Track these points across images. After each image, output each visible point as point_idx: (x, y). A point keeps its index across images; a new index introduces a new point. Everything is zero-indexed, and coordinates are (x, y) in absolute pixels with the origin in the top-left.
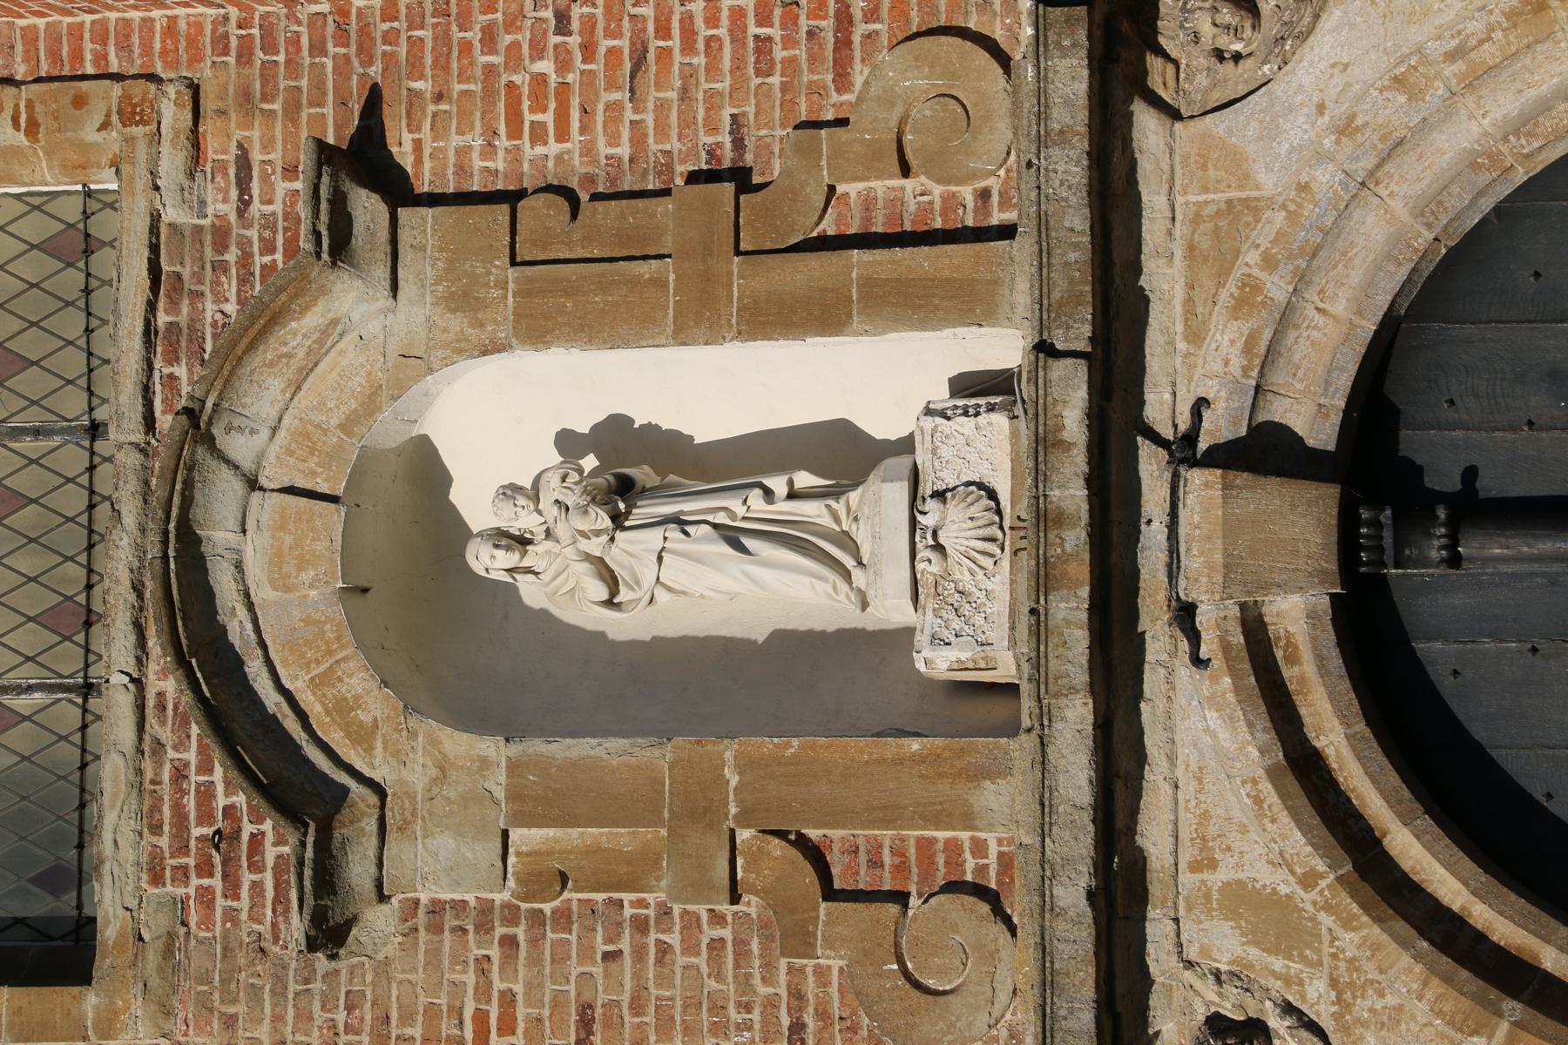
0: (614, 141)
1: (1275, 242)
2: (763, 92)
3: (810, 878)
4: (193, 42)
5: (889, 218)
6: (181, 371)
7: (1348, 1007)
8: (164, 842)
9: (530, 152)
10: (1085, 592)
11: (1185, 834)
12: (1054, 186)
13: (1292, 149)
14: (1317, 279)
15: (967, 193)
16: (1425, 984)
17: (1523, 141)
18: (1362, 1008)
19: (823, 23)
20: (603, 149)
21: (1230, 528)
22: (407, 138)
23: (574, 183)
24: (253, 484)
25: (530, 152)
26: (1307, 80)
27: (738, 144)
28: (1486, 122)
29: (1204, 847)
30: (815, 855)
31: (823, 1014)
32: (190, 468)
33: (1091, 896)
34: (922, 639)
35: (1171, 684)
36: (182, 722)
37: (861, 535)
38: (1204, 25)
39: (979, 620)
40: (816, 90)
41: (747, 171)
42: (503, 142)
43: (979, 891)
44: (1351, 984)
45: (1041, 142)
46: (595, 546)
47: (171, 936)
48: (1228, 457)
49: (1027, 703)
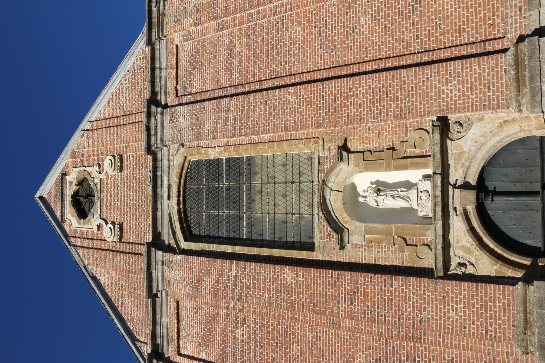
0: (376, 144)
2: (396, 137)
3: (404, 243)
4: (323, 133)
5: (413, 154)
6: (322, 175)
7: (477, 262)
8: (322, 234)
9: (366, 146)
10: (441, 206)
11: (455, 238)
15: (424, 151)
18: (479, 262)
20: (375, 145)
21: (461, 197)
22: (350, 144)
23: (371, 150)
24: (331, 190)
25: (366, 146)
26: (470, 136)
27: (393, 144)
29: (458, 240)
30: (405, 240)
31: (406, 260)
32: (323, 188)
33: (442, 247)
34: (419, 211)
35: (453, 218)
36: (323, 220)
37: (411, 197)
38: (456, 128)
39: (427, 209)
40: (403, 137)
41: (394, 148)
42: (362, 145)
43: (427, 245)
45: (433, 145)
46: (375, 198)
47: (323, 246)
48: (461, 187)
49: (433, 219)
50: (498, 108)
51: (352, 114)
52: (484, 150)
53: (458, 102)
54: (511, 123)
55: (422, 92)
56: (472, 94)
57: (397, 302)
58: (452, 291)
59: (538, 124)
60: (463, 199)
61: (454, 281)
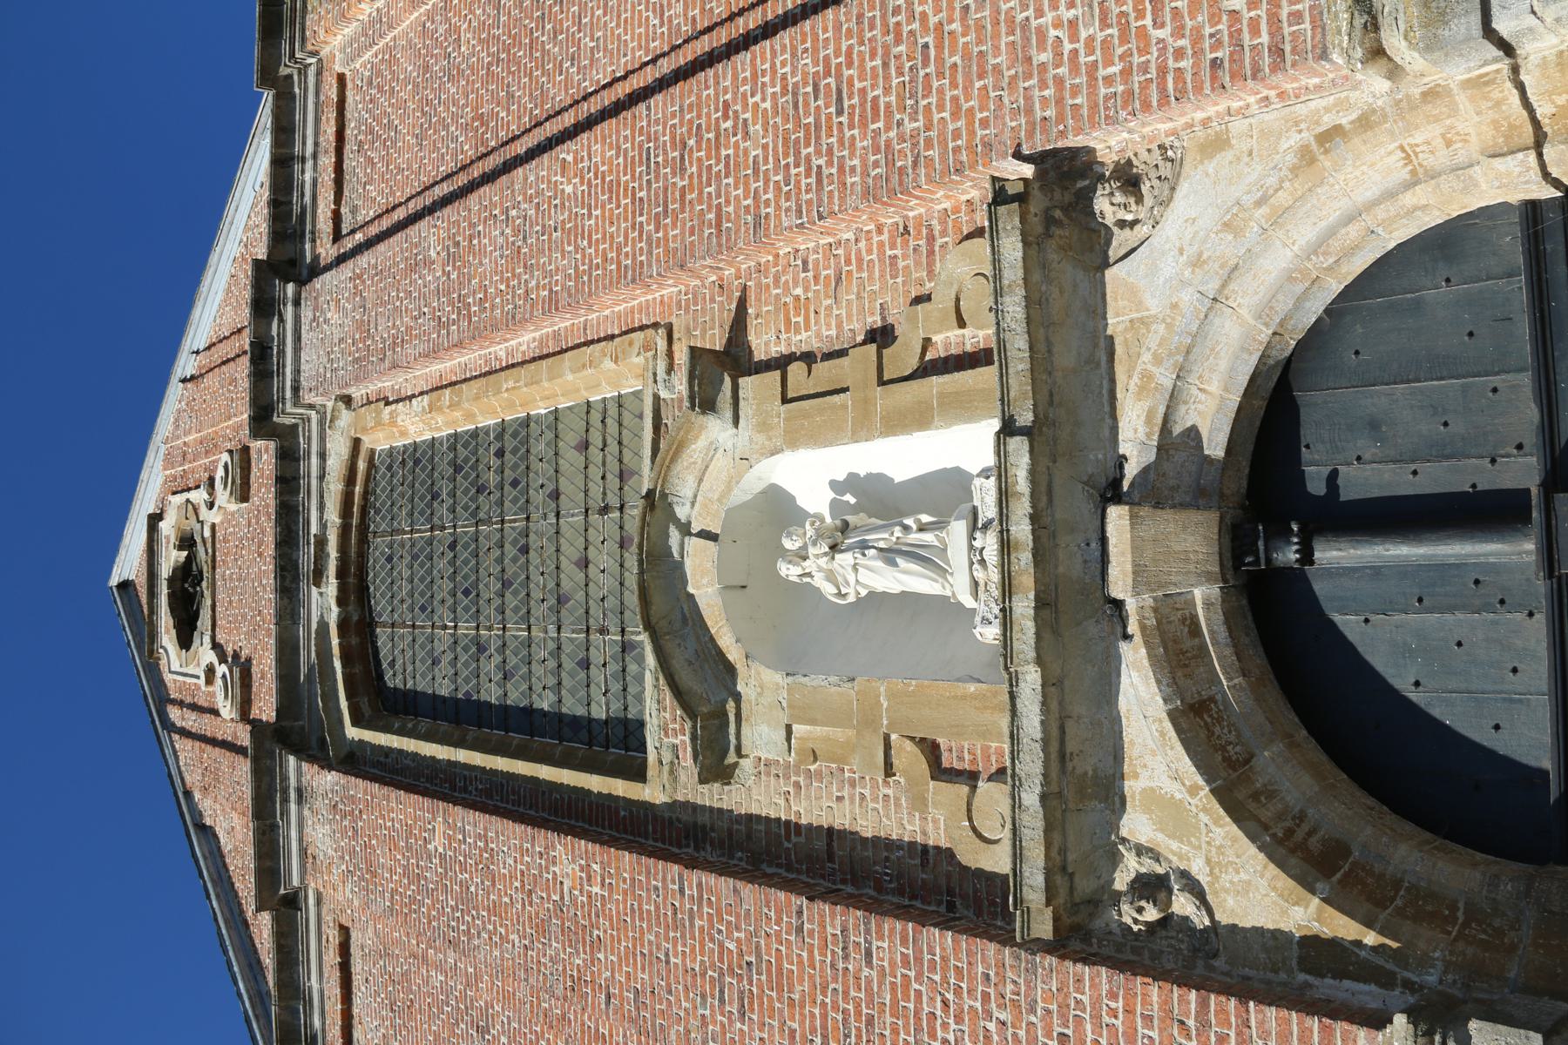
1: (1160, 345)
7: (1217, 878)
12: (1008, 321)
13: (1166, 281)
14: (1195, 368)
16: (1265, 867)
17: (1322, 259)
19: (920, 243)
28: (1295, 248)
42: (783, 336)
44: (1219, 863)
50: (1275, 68)
51: (731, 209)
52: (1248, 297)
53: (1102, 73)
54: (1356, 141)
55: (959, 62)
56: (1158, 24)
57: (887, 1033)
58: (1097, 1017)
59: (1495, 124)
60: (1148, 554)
61: (1103, 970)
